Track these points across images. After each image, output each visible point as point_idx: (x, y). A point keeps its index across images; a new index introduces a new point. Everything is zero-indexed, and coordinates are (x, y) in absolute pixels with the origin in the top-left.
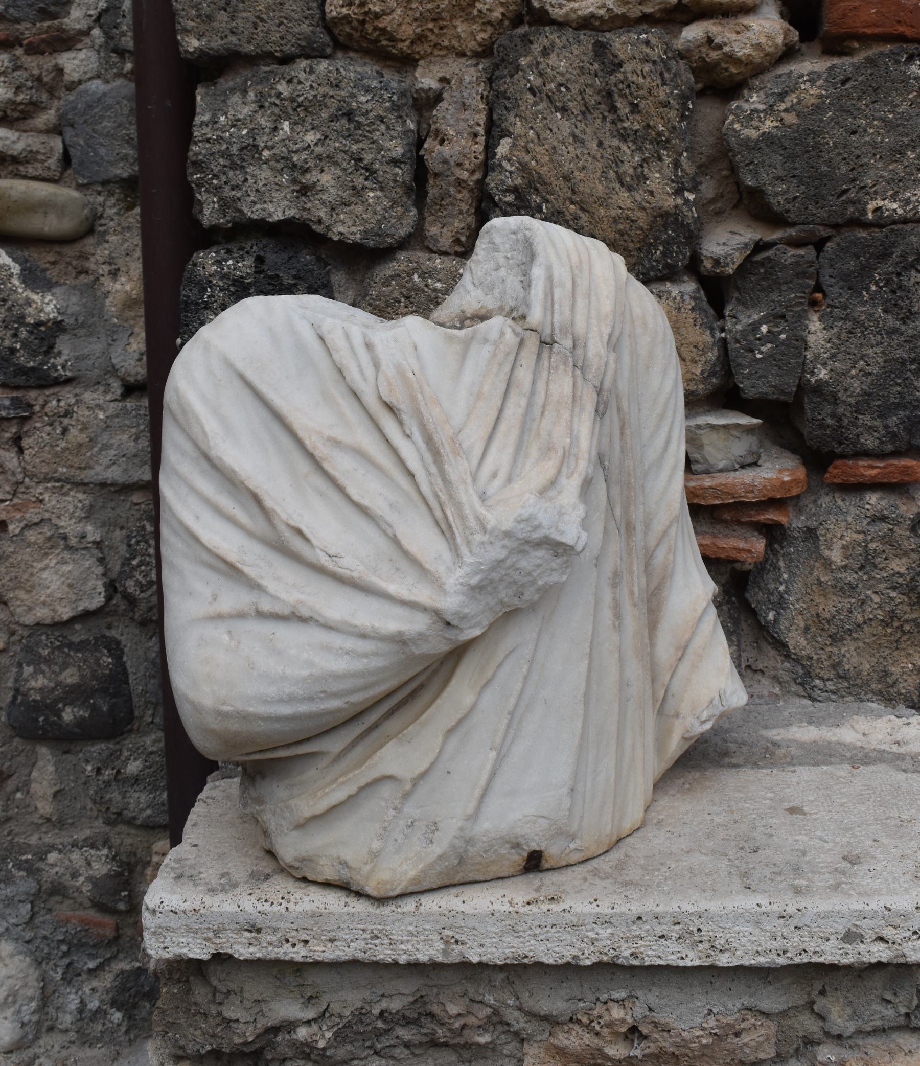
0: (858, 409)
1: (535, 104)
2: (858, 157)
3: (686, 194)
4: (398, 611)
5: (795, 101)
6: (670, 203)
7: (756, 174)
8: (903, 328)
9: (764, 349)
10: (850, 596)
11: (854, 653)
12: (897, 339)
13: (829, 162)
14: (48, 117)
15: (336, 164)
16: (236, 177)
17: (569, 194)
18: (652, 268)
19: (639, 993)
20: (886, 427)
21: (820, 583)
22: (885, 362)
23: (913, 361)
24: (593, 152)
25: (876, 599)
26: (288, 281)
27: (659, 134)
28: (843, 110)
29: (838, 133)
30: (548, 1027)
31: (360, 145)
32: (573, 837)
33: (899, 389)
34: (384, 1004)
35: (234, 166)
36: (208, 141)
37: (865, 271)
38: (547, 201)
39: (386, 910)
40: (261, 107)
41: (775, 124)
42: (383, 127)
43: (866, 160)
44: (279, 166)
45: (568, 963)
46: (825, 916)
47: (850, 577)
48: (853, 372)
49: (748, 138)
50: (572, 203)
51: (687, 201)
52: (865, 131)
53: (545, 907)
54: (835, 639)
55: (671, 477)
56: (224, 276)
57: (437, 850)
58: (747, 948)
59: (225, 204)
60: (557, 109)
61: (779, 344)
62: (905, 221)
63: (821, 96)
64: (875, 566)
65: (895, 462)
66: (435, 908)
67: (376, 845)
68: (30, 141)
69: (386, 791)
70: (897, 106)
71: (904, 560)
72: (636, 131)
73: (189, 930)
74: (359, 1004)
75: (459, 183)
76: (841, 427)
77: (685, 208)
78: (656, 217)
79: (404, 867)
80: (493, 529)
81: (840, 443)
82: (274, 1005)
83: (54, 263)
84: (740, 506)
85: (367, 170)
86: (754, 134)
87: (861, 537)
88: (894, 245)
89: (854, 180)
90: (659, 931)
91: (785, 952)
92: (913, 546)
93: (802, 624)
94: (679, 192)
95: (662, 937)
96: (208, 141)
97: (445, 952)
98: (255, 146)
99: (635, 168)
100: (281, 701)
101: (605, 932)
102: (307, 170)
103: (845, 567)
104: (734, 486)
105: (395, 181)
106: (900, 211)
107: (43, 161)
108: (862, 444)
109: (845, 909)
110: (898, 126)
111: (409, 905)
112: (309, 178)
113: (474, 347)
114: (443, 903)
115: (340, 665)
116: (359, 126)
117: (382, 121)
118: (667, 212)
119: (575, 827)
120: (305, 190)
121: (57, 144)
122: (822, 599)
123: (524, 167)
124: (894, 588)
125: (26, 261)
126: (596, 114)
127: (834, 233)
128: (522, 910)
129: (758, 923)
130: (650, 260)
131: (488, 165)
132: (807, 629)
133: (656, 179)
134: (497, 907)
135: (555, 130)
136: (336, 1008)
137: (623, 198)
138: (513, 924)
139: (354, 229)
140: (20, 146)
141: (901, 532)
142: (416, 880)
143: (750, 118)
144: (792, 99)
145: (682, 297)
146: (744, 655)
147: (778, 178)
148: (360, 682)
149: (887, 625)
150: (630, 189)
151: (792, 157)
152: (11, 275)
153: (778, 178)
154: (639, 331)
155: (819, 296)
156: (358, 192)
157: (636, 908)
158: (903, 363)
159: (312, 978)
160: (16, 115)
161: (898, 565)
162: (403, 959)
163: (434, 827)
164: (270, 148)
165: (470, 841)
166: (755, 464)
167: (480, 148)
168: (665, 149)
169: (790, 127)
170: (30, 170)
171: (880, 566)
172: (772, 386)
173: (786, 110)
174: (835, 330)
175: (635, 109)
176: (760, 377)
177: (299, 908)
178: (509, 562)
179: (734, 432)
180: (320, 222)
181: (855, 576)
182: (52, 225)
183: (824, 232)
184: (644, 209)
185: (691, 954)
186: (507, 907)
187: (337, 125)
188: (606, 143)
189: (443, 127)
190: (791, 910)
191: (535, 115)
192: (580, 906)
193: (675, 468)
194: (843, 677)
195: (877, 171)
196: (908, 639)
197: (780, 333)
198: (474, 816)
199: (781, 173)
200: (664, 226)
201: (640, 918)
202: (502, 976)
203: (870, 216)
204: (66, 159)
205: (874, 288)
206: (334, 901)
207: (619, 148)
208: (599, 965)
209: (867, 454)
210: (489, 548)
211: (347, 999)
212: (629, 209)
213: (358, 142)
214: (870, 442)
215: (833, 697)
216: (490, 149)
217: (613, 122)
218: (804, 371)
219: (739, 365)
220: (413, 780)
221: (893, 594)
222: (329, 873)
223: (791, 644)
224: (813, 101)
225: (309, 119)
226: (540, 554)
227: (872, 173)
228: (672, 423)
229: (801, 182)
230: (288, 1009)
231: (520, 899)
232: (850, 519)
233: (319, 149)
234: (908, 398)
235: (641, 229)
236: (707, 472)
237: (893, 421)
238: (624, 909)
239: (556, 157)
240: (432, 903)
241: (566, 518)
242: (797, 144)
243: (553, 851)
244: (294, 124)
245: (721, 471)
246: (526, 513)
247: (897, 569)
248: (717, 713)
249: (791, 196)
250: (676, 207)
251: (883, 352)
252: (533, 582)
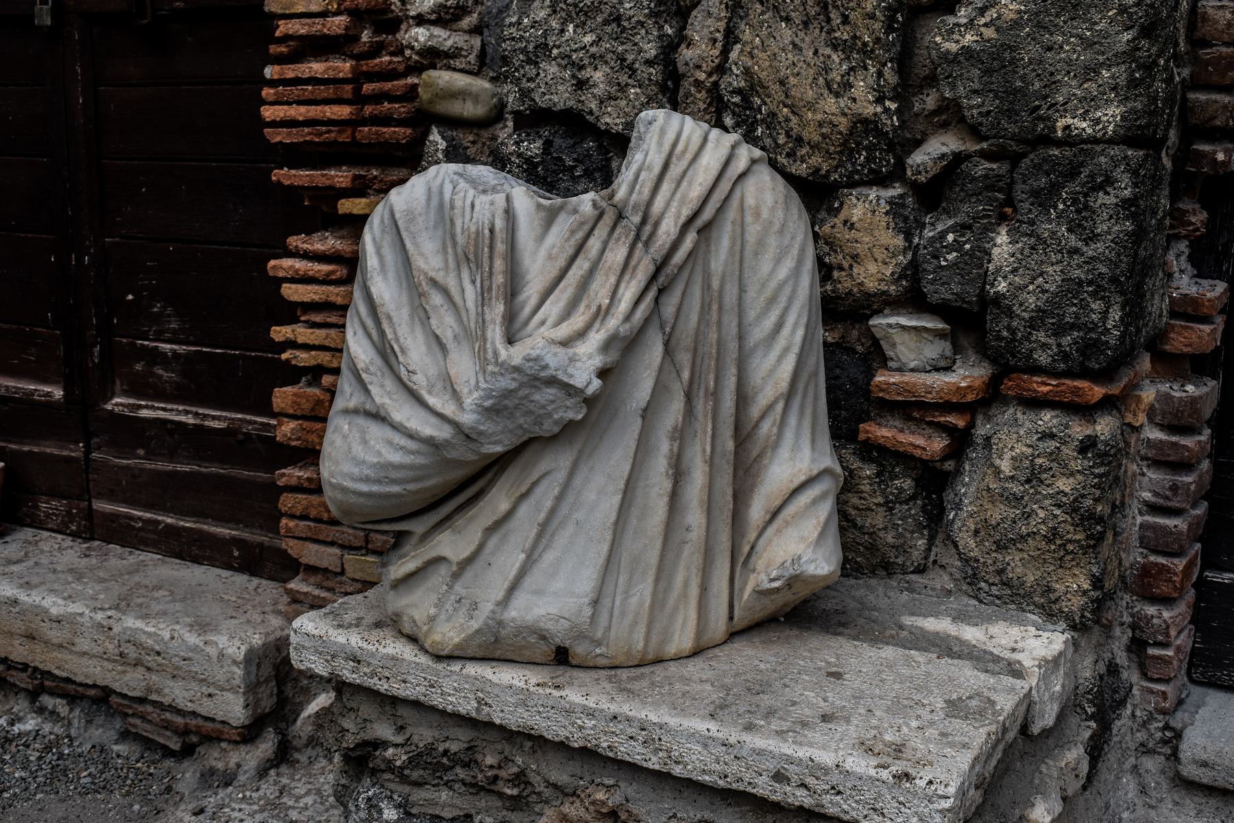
0: (1033, 324)
1: (763, 13)
2: (1052, 74)
3: (887, 103)
4: (434, 420)
5: (995, 15)
6: (870, 110)
7: (953, 87)
8: (1085, 249)
9: (949, 257)
10: (1015, 507)
11: (1019, 564)
12: (1077, 259)
13: (1023, 78)
14: (467, 22)
15: (606, 62)
16: (530, 70)
17: (783, 98)
18: (857, 172)
19: (621, 784)
20: (1059, 345)
21: (989, 489)
22: (1063, 280)
23: (1090, 283)
24: (808, 59)
25: (1042, 514)
26: (471, 151)
27: (865, 44)
28: (1040, 25)
29: (1034, 50)
30: (561, 797)
31: (625, 47)
32: (599, 643)
33: (1075, 309)
34: (447, 745)
35: (529, 61)
36: (513, 39)
37: (1054, 189)
38: (765, 104)
39: (440, 666)
40: (555, 12)
41: (975, 38)
42: (643, 31)
43: (1059, 77)
44: (563, 63)
45: (562, 742)
46: (760, 752)
47: (1016, 488)
48: (1031, 288)
49: (948, 51)
50: (785, 106)
51: (887, 110)
52: (1061, 47)
53: (548, 691)
54: (1000, 547)
55: (780, 358)
56: (520, 155)
57: (475, 625)
58: (696, 762)
59: (525, 94)
60: (782, 19)
61: (963, 254)
62: (1094, 140)
63: (1019, 12)
64: (1042, 482)
65: (1068, 382)
66: (473, 673)
67: (433, 611)
68: (457, 39)
69: (443, 571)
70: (1096, 23)
71: (1071, 480)
72: (846, 41)
73: (316, 651)
74: (430, 740)
75: (698, 83)
76: (1014, 340)
77: (883, 117)
78: (855, 123)
79: (451, 634)
80: (503, 363)
81: (1014, 356)
82: (376, 726)
83: (473, 142)
84: (922, 406)
85: (630, 69)
86: (953, 47)
87: (1030, 450)
88: (1082, 164)
89: (1046, 97)
90: (630, 731)
91: (726, 777)
92: (1080, 468)
93: (973, 527)
94: (879, 100)
95: (631, 738)
96: (513, 39)
97: (478, 710)
98: (547, 45)
99: (843, 76)
100: (361, 480)
101: (590, 723)
102: (582, 68)
103: (1012, 477)
104: (915, 385)
105: (650, 80)
106: (1089, 131)
107: (466, 57)
108: (1035, 360)
109: (776, 751)
110: (1095, 43)
111: (456, 667)
112: (584, 74)
113: (562, 217)
114: (479, 671)
115: (396, 457)
116: (624, 30)
117: (643, 26)
118: (866, 119)
119: (599, 634)
120: (581, 85)
121: (477, 42)
122: (990, 506)
123: (747, 72)
124: (1059, 506)
125: (454, 139)
126: (816, 23)
127: (1029, 148)
128: (532, 689)
129: (705, 746)
130: (854, 164)
131: (721, 69)
132: (977, 532)
133: (861, 87)
134: (516, 682)
135: (778, 38)
136: (415, 738)
137: (830, 104)
138: (524, 698)
139: (618, 121)
140: (449, 43)
141: (1068, 451)
142: (459, 646)
143: (951, 32)
144: (993, 13)
145: (878, 200)
146: (934, 549)
147: (975, 92)
148: (410, 474)
149: (1050, 541)
150: (837, 95)
151: (988, 72)
152: (437, 150)
153: (975, 92)
154: (749, 219)
155: (1009, 210)
156: (623, 88)
157: (614, 708)
158: (1080, 283)
159: (402, 711)
160: (448, 17)
161: (1064, 484)
162: (450, 708)
163: (475, 606)
164: (558, 47)
165: (500, 623)
166: (948, 369)
167: (716, 52)
168: (870, 59)
169: (988, 41)
170: (457, 63)
171: (1047, 482)
172: (953, 294)
173: (986, 25)
174: (1020, 245)
175: (846, 20)
176: (943, 284)
177: (385, 651)
178: (521, 393)
179: (925, 335)
180: (591, 113)
181: (1021, 488)
182: (469, 110)
183: (1020, 148)
184: (845, 115)
185: (654, 759)
186: (522, 684)
187: (608, 29)
188: (820, 51)
189: (690, 33)
190: (732, 740)
191: (761, 23)
192: (574, 696)
193: (786, 350)
194: (1006, 584)
195: (1070, 88)
196: (1073, 560)
197: (965, 243)
198: (505, 602)
199: (976, 86)
200: (864, 132)
201: (615, 717)
202: (529, 744)
203: (1060, 134)
204: (482, 54)
205: (1061, 207)
206: (406, 651)
207: (829, 57)
208: (584, 750)
209: (1037, 370)
210: (500, 378)
211: (424, 734)
212: (833, 114)
213: (623, 43)
214: (1043, 358)
215: (997, 602)
216: (725, 52)
217: (828, 33)
218: (985, 283)
219: (925, 270)
220: (459, 563)
221: (1057, 512)
222: (407, 628)
223: (961, 544)
224: (1012, 16)
225: (589, 23)
226: (551, 392)
227: (1064, 90)
228: (786, 310)
229: (996, 97)
230: (383, 731)
231: (533, 681)
232: (1022, 432)
233: (593, 49)
234: (1083, 319)
235: (841, 133)
236: (900, 370)
237: (1066, 340)
238: (605, 707)
239: (776, 64)
240: (472, 669)
241: (578, 364)
242: (994, 59)
243: (580, 650)
244: (576, 26)
245: (912, 370)
246: (534, 353)
247: (1062, 488)
248: (787, 574)
249: (984, 109)
250: (875, 114)
251: (1061, 271)
252: (550, 415)
